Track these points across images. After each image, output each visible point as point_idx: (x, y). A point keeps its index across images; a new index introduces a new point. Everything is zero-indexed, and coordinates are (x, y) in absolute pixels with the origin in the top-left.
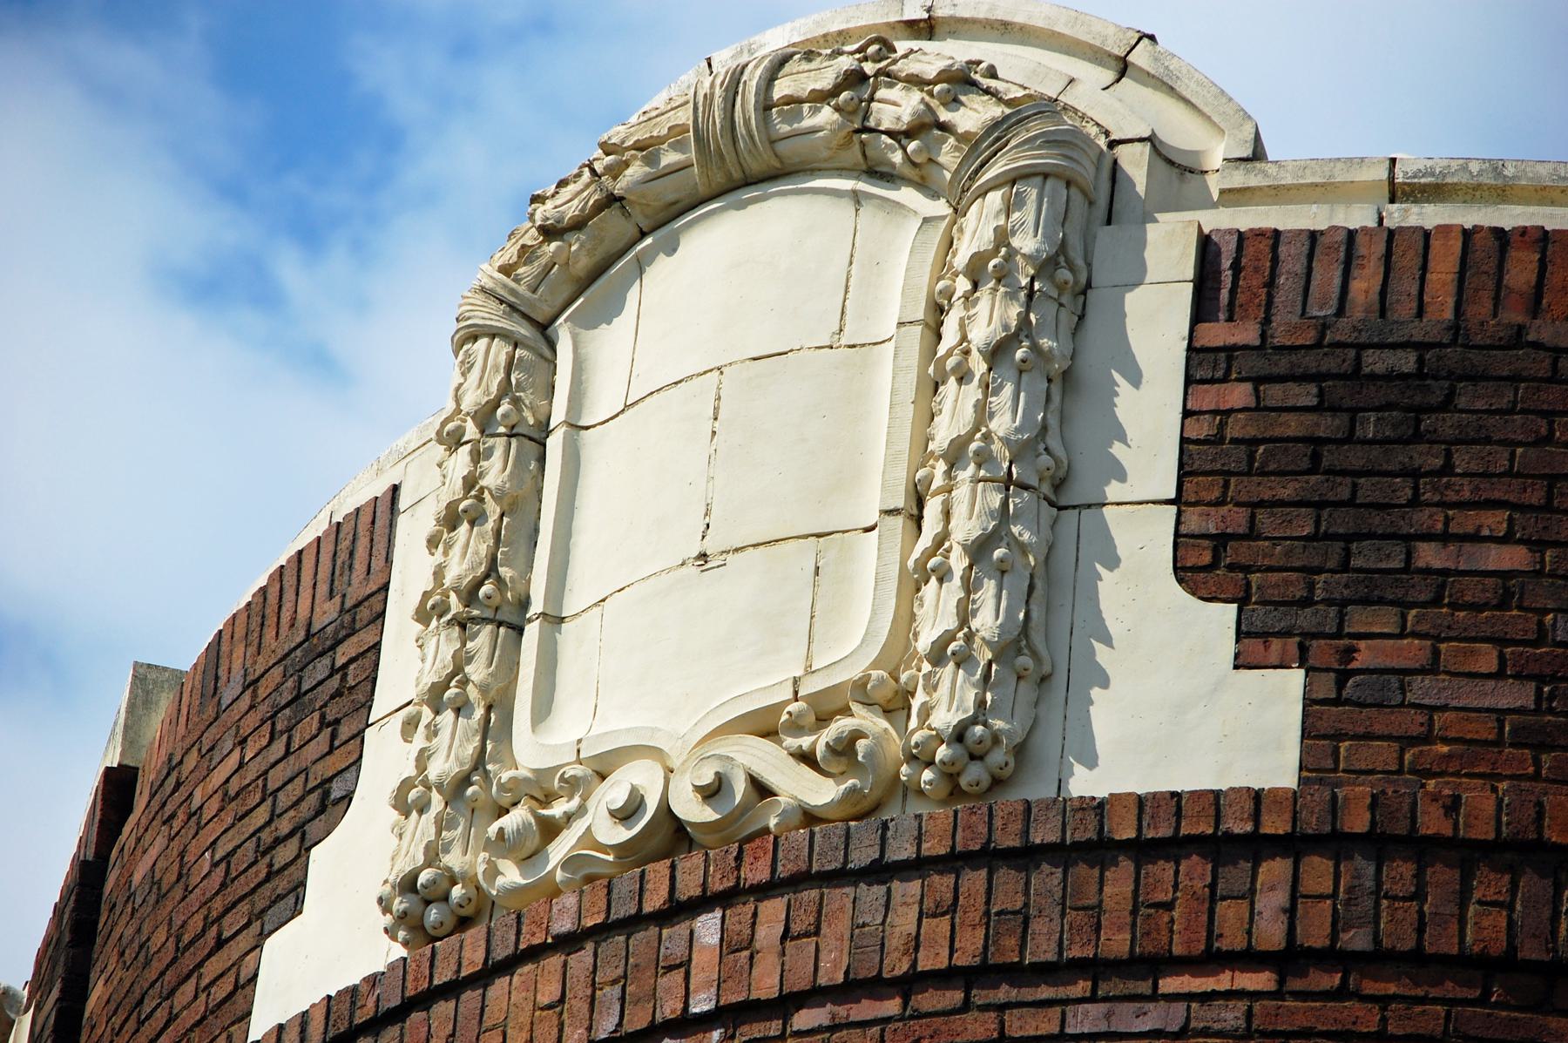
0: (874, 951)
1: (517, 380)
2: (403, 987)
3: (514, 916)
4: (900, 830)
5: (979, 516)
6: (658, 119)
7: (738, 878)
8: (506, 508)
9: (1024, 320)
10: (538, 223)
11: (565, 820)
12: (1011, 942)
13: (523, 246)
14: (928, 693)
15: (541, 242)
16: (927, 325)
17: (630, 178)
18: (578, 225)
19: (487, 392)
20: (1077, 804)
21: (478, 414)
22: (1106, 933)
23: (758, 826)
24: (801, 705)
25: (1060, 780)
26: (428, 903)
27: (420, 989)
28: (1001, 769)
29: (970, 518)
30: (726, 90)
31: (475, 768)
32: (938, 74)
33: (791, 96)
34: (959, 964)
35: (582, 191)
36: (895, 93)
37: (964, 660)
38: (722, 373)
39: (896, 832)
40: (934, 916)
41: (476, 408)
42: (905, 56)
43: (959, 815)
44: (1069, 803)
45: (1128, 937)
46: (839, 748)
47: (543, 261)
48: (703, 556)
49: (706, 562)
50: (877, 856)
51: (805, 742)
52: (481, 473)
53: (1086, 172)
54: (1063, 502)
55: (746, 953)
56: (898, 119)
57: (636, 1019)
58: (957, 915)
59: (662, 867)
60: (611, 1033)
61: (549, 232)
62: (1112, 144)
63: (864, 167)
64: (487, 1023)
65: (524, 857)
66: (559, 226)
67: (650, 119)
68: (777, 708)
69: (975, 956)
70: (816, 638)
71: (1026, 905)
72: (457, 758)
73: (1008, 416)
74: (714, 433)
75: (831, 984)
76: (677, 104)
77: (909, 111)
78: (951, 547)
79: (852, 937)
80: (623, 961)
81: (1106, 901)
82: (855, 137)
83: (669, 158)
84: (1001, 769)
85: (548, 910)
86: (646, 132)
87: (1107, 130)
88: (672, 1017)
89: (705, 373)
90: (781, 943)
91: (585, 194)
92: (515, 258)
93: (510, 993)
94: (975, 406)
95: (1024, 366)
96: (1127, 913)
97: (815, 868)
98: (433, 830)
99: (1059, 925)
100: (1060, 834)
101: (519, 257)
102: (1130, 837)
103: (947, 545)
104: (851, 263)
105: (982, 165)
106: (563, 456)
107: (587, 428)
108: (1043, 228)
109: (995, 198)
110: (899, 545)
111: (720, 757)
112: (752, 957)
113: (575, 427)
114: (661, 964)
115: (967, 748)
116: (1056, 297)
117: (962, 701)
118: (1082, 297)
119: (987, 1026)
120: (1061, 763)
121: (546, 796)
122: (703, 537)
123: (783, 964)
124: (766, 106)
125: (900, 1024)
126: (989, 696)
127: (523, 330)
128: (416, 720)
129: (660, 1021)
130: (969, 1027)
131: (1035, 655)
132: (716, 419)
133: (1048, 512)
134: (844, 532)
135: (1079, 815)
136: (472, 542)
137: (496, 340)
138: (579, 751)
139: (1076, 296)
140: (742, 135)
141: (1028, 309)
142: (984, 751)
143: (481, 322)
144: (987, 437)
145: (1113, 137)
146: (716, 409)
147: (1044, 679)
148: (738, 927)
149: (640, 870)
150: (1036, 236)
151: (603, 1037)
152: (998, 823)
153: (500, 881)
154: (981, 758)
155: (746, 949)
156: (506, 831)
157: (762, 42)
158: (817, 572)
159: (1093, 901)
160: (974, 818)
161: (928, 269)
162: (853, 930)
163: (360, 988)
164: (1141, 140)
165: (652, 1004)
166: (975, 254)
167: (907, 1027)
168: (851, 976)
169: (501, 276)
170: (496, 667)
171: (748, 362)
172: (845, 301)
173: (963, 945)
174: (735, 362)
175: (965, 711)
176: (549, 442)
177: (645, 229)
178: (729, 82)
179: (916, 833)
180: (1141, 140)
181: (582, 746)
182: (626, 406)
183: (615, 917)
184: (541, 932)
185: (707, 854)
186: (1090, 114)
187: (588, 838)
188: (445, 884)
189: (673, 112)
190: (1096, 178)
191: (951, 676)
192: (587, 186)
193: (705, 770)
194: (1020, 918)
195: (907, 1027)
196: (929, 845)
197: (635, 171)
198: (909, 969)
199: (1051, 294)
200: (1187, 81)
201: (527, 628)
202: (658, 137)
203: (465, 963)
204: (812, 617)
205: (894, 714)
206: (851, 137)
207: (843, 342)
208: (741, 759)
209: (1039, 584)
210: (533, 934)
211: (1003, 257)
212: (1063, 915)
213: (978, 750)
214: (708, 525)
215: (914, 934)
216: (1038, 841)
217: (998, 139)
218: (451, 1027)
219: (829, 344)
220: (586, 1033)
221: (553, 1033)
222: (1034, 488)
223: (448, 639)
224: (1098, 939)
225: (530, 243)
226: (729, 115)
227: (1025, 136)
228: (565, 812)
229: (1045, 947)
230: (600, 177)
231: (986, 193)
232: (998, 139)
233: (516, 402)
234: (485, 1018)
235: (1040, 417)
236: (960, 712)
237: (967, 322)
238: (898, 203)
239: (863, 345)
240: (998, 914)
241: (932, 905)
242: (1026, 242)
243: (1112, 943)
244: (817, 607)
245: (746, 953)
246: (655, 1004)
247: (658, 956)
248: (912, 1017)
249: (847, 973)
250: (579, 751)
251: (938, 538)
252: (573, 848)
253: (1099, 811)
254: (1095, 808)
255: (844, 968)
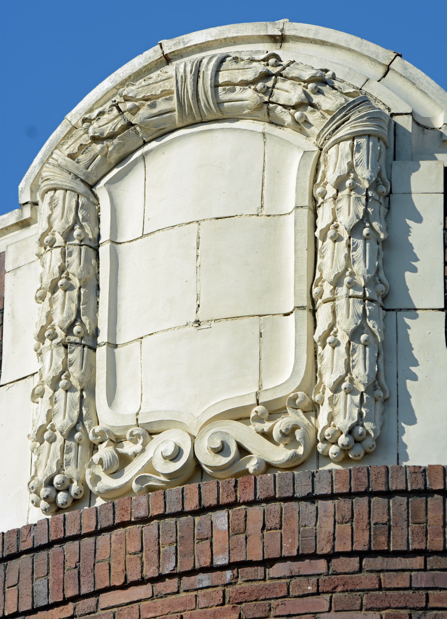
0: (312, 540)
1: (83, 216)
2: (48, 534)
3: (111, 505)
4: (322, 478)
5: (353, 317)
6: (154, 85)
7: (236, 496)
8: (82, 284)
9: (366, 212)
10: (91, 134)
11: (134, 456)
12: (383, 539)
13: (81, 145)
14: (331, 407)
15: (90, 143)
16: (310, 208)
17: (141, 116)
18: (112, 137)
19: (67, 222)
20: (412, 470)
21: (64, 233)
22: (430, 537)
23: (241, 469)
24: (259, 408)
25: (398, 454)
26: (58, 491)
27: (59, 537)
28: (370, 448)
29: (348, 317)
30: (194, 75)
31: (78, 423)
32: (310, 78)
33: (230, 81)
34: (357, 549)
35: (114, 119)
36: (287, 85)
37: (351, 391)
38: (199, 224)
39: (320, 479)
40: (342, 523)
41: (63, 230)
42: (288, 65)
43: (352, 472)
44: (408, 469)
45: (442, 539)
46: (287, 433)
47: (93, 153)
48: (197, 321)
49: (199, 325)
50: (310, 491)
51: (266, 426)
52: (68, 265)
53: (384, 133)
54: (387, 307)
55: (243, 536)
56: (290, 99)
57: (184, 565)
58: (354, 523)
59: (194, 486)
60: (172, 571)
61: (95, 139)
62: (392, 115)
63: (268, 120)
64: (98, 558)
65: (111, 472)
66: (101, 137)
67: (149, 84)
68: (249, 408)
69: (364, 546)
70: (263, 370)
71: (389, 520)
72: (70, 417)
73: (362, 263)
74: (198, 256)
75: (290, 555)
76: (164, 78)
77: (296, 96)
78: (337, 331)
79: (299, 531)
80: (175, 534)
81: (430, 520)
82: (265, 106)
83: (162, 106)
84: (370, 448)
85: (130, 503)
86: (148, 92)
87: (389, 108)
88: (204, 566)
89: (190, 223)
90: (262, 532)
91: (116, 121)
92: (76, 150)
93: (110, 544)
94: (345, 257)
95: (368, 237)
96: (441, 527)
97: (277, 496)
98: (59, 454)
99: (407, 531)
100: (405, 485)
101: (79, 150)
102: (441, 488)
103: (335, 329)
104: (264, 171)
105: (337, 128)
106: (110, 258)
107: (120, 243)
108: (371, 164)
109: (345, 146)
110: (306, 326)
111: (222, 433)
112: (246, 538)
113: (114, 242)
114: (196, 537)
115: (354, 437)
116: (378, 199)
117: (351, 414)
118: (388, 198)
119: (372, 581)
120: (398, 445)
121: (116, 439)
122: (197, 312)
123: (263, 543)
124: (216, 86)
125: (327, 577)
126: (363, 410)
127: (82, 188)
128: (42, 393)
129: (199, 567)
130: (363, 581)
131: (383, 389)
132: (198, 248)
133: (383, 312)
134: (273, 315)
135: (414, 475)
136: (66, 302)
137: (68, 191)
138: (137, 420)
139: (385, 197)
140: (203, 99)
141: (366, 206)
142: (362, 439)
143: (60, 183)
144: (352, 274)
145: (392, 112)
146: (198, 244)
147: (386, 401)
148: (237, 522)
149: (181, 487)
150: (368, 168)
151: (167, 572)
152: (372, 477)
153: (99, 484)
154: (360, 442)
155: (243, 533)
156: (104, 460)
157: (190, 39)
158: (261, 336)
159: (423, 520)
160: (360, 474)
161: (308, 179)
162: (299, 528)
163: (22, 531)
164: (406, 114)
165: (193, 558)
166: (338, 177)
167: (331, 579)
168: (300, 552)
169: (70, 160)
170: (85, 369)
171: (213, 220)
172: (262, 191)
173: (358, 539)
174: (207, 219)
175: (353, 419)
176: (101, 249)
177: (146, 141)
178: (195, 71)
179: (330, 480)
180: (406, 114)
181: (139, 417)
182: (143, 235)
183: (169, 512)
184: (127, 515)
185: (218, 483)
186: (379, 98)
187: (149, 466)
188: (67, 483)
189: (162, 83)
190: (388, 134)
191: (344, 399)
192: (116, 117)
193: (215, 439)
194: (387, 527)
195: (331, 579)
196: (338, 487)
197: (144, 112)
198: (331, 551)
199: (376, 198)
200: (422, 81)
201: (98, 349)
202: (155, 95)
203: (84, 526)
204: (260, 360)
205: (307, 413)
206: (263, 105)
207: (264, 213)
208: (232, 434)
209: (382, 352)
210: (123, 515)
211: (353, 179)
212: (408, 526)
213: (359, 438)
214: (199, 306)
215: (332, 532)
216: (394, 488)
217: (345, 115)
218: (78, 557)
219: (257, 213)
220: (157, 570)
221: (138, 567)
222: (376, 301)
223: (58, 353)
224: (427, 539)
225: (84, 143)
226: (195, 88)
227: (358, 115)
228: (134, 452)
229: (400, 542)
230: (123, 113)
231: (339, 143)
232: (345, 115)
233: (82, 227)
234: (97, 555)
235: (377, 264)
236: (351, 420)
237: (336, 212)
238: (288, 142)
239: (274, 216)
240: (375, 524)
241: (341, 518)
242: (364, 172)
243: (434, 542)
244: (262, 354)
245: (243, 536)
246: (194, 558)
247: (194, 533)
248: (333, 574)
249: (298, 550)
250: (137, 420)
251: (330, 326)
252: (139, 472)
253: (423, 474)
254: (422, 472)
255: (297, 548)
